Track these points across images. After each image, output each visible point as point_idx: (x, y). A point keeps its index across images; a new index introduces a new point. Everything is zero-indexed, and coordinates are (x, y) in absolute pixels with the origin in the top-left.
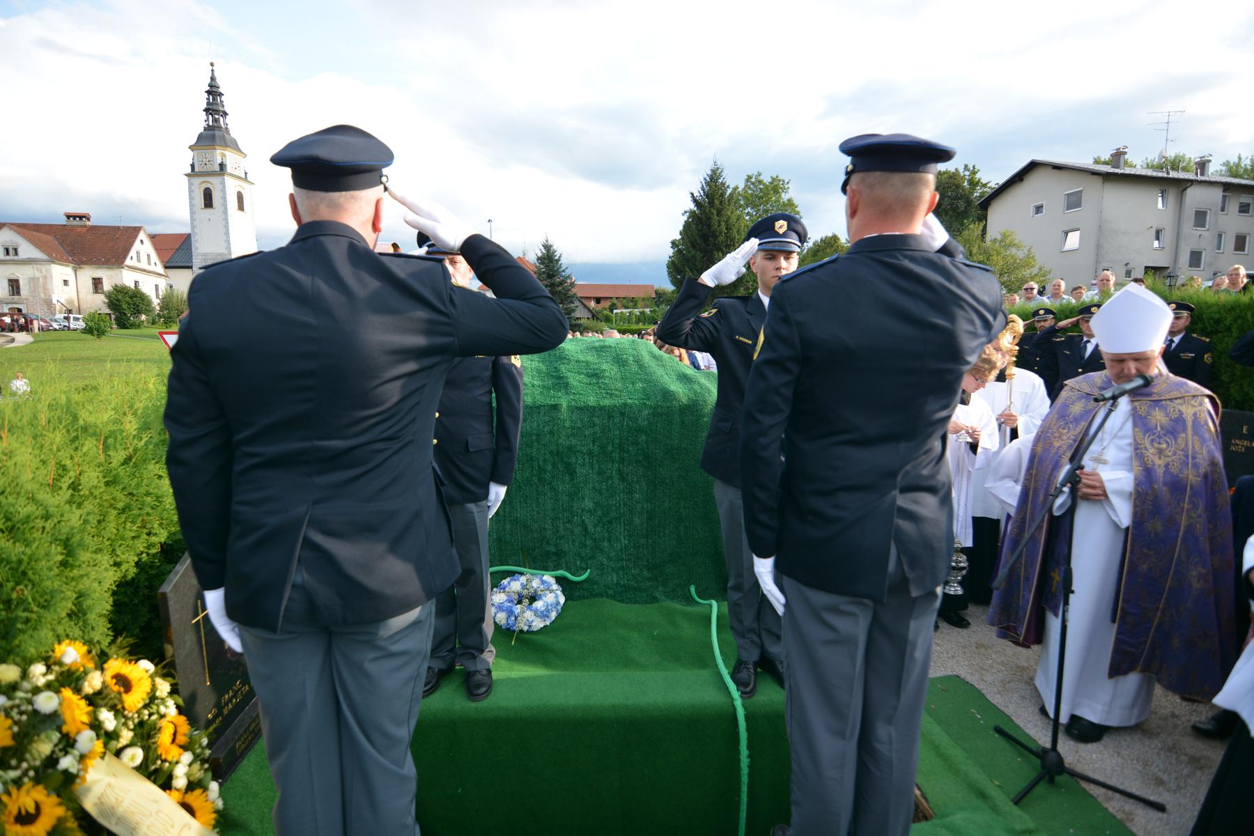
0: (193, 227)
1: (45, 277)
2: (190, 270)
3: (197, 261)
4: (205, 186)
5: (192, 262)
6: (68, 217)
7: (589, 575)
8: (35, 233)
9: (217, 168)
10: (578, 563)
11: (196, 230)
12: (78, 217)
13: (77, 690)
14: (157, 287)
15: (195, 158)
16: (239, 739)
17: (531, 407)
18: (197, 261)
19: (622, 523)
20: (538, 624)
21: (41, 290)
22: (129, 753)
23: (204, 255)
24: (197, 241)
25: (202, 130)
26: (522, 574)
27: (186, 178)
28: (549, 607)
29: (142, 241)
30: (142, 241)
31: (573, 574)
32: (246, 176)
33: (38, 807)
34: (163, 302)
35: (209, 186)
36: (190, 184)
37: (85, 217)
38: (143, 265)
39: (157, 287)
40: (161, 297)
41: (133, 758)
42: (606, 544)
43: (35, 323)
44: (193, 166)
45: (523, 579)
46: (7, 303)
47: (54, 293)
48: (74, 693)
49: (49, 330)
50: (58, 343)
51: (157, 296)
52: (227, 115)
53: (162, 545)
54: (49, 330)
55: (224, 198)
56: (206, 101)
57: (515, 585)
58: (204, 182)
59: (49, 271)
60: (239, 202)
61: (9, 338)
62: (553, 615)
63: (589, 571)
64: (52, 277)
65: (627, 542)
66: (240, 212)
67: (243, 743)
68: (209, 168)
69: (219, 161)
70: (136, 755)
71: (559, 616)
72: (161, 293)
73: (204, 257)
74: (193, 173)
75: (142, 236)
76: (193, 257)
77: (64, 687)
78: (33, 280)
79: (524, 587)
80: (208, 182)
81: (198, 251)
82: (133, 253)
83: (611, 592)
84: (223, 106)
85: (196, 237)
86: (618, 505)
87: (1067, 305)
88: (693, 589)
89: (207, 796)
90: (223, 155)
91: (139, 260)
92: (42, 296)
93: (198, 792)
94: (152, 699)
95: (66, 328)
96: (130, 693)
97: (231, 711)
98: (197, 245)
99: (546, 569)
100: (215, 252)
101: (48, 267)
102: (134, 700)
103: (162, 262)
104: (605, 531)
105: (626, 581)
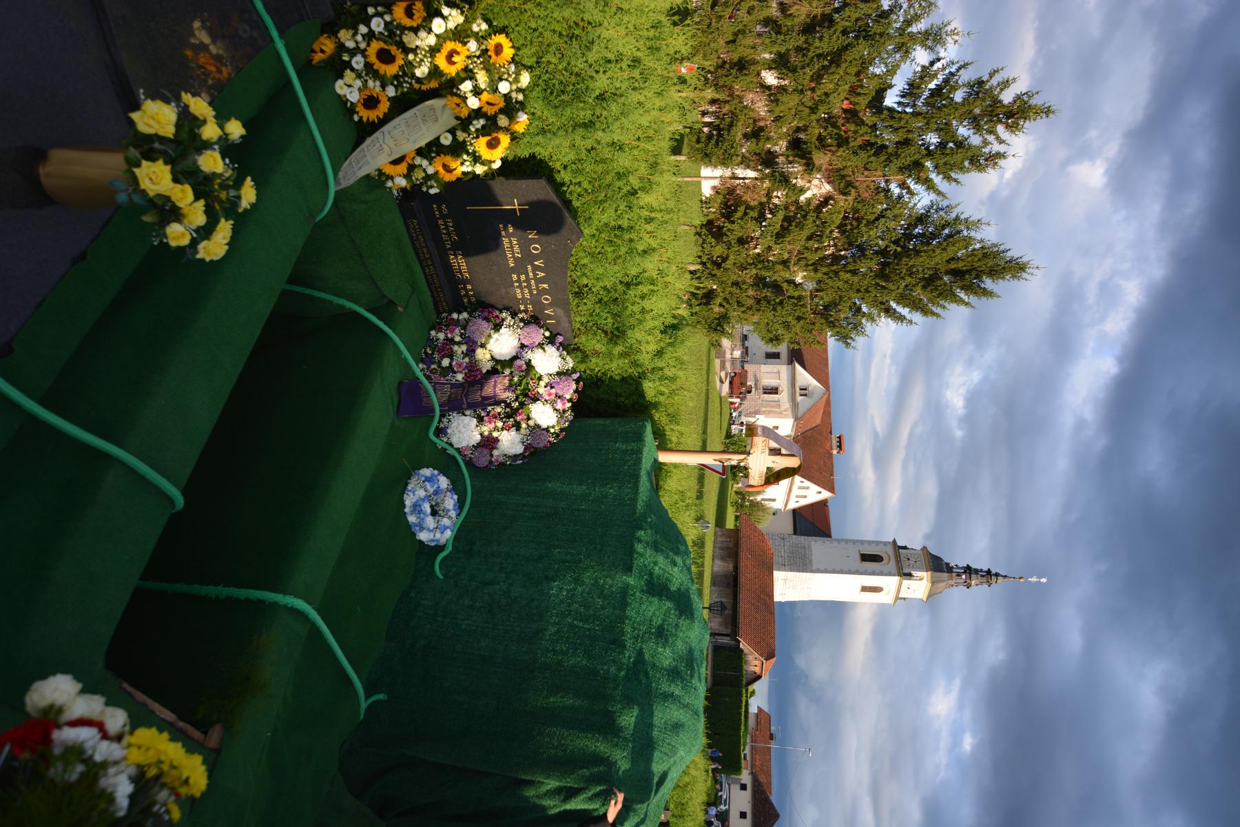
0: (839, 541)
1: (780, 413)
2: (792, 532)
3: (803, 541)
4: (885, 557)
5: (801, 535)
6: (839, 437)
7: (438, 577)
8: (822, 411)
9: (906, 571)
10: (454, 570)
11: (835, 543)
12: (840, 444)
13: (501, 111)
14: (774, 500)
15: (913, 551)
16: (419, 224)
17: (631, 548)
18: (803, 541)
19: (487, 625)
20: (409, 501)
21: (768, 409)
22: (450, 137)
23: (810, 546)
24: (824, 542)
25: (945, 561)
26: (458, 515)
27: (891, 540)
28: (422, 515)
29: (820, 492)
30: (820, 492)
31: (444, 559)
32: (901, 598)
33: (454, 63)
34: (758, 503)
35: (885, 561)
36: (885, 544)
37: (841, 449)
38: (795, 491)
39: (774, 500)
40: (763, 502)
41: (446, 138)
42: (467, 602)
43: (738, 400)
44: (905, 548)
45: (453, 514)
46: (756, 384)
47: (765, 417)
48: (501, 108)
49: (731, 410)
50: (719, 410)
51: (763, 500)
52: (968, 588)
53: (571, 201)
54: (731, 410)
55: (873, 573)
56: (979, 568)
57: (450, 502)
58: (889, 556)
59: (786, 416)
60: (870, 587)
61: (724, 380)
62: (412, 519)
63: (441, 577)
64: (781, 418)
65: (464, 627)
66: (860, 588)
67: (414, 228)
68: (905, 563)
69: (914, 573)
70: (446, 140)
71: (408, 526)
72: (767, 503)
73: (806, 547)
74: (897, 548)
75: (826, 494)
76: (806, 537)
77: (505, 106)
78: (778, 404)
79: (447, 511)
80: (889, 560)
81: (813, 543)
82: (807, 483)
83: (413, 594)
84: (977, 585)
85: (828, 542)
86: (508, 623)
87: (746, 661)
88: (381, 696)
89: (400, 176)
90: (921, 579)
91: (800, 488)
92: (763, 409)
93: (405, 171)
94: (476, 159)
95: (732, 422)
96: (487, 149)
97: (438, 226)
98: (819, 542)
99: (457, 538)
100: (813, 557)
101: (791, 415)
102: (481, 145)
103: (800, 508)
104: (482, 604)
105: (419, 614)
